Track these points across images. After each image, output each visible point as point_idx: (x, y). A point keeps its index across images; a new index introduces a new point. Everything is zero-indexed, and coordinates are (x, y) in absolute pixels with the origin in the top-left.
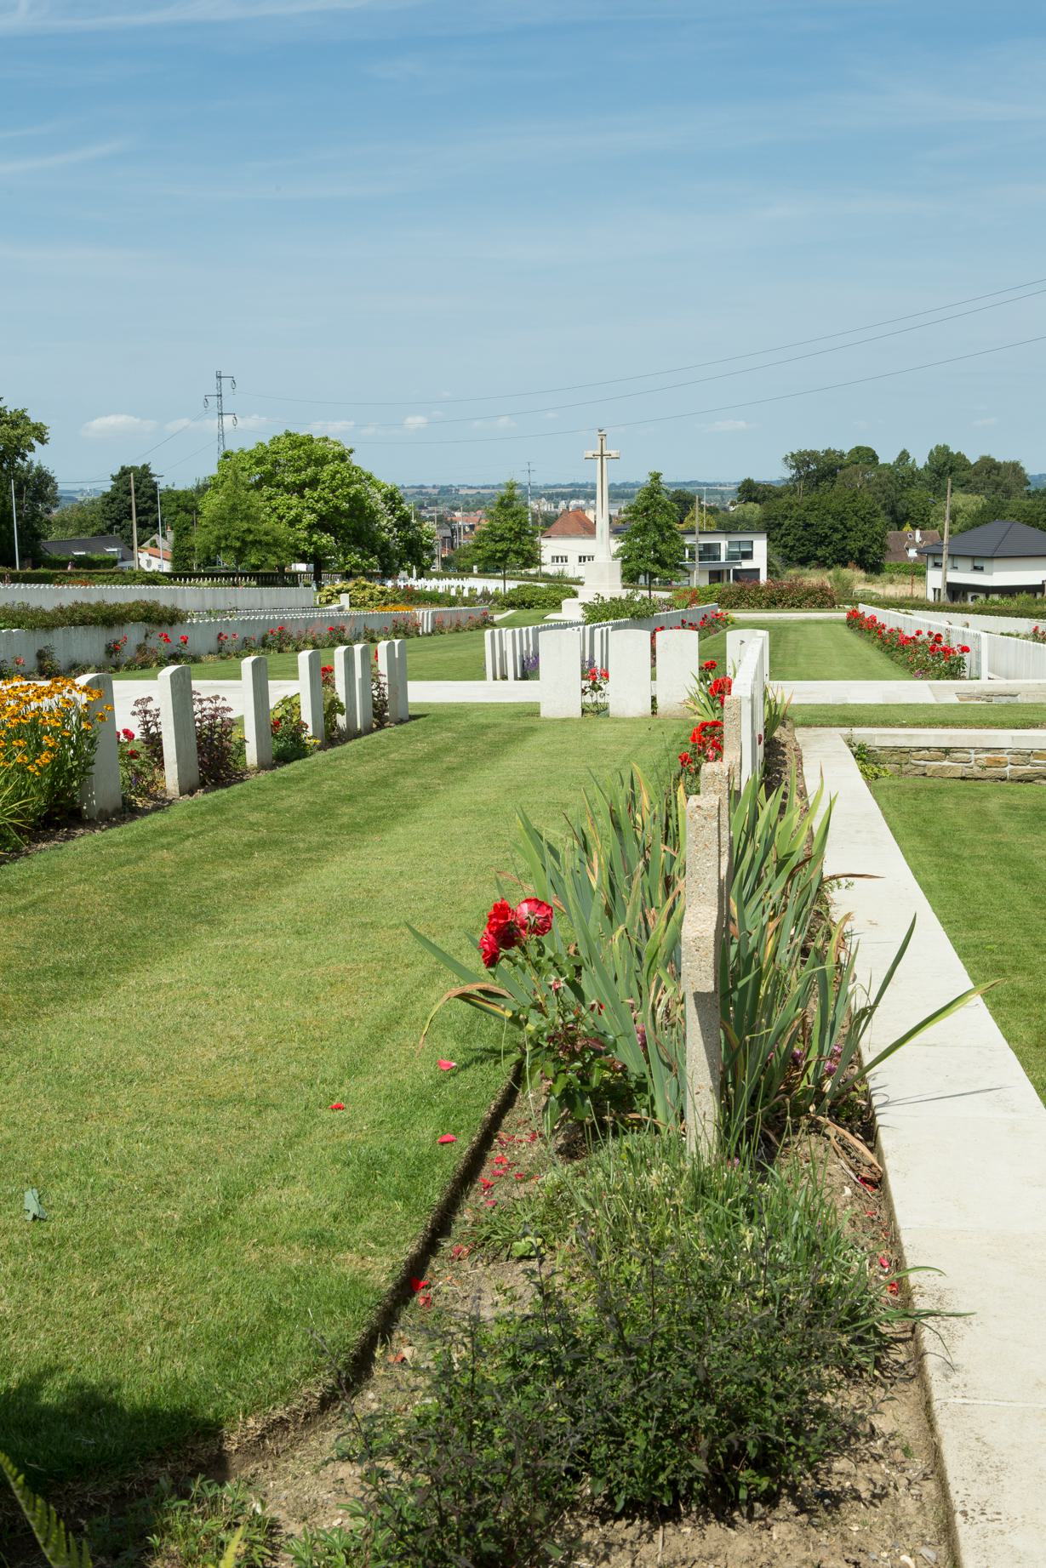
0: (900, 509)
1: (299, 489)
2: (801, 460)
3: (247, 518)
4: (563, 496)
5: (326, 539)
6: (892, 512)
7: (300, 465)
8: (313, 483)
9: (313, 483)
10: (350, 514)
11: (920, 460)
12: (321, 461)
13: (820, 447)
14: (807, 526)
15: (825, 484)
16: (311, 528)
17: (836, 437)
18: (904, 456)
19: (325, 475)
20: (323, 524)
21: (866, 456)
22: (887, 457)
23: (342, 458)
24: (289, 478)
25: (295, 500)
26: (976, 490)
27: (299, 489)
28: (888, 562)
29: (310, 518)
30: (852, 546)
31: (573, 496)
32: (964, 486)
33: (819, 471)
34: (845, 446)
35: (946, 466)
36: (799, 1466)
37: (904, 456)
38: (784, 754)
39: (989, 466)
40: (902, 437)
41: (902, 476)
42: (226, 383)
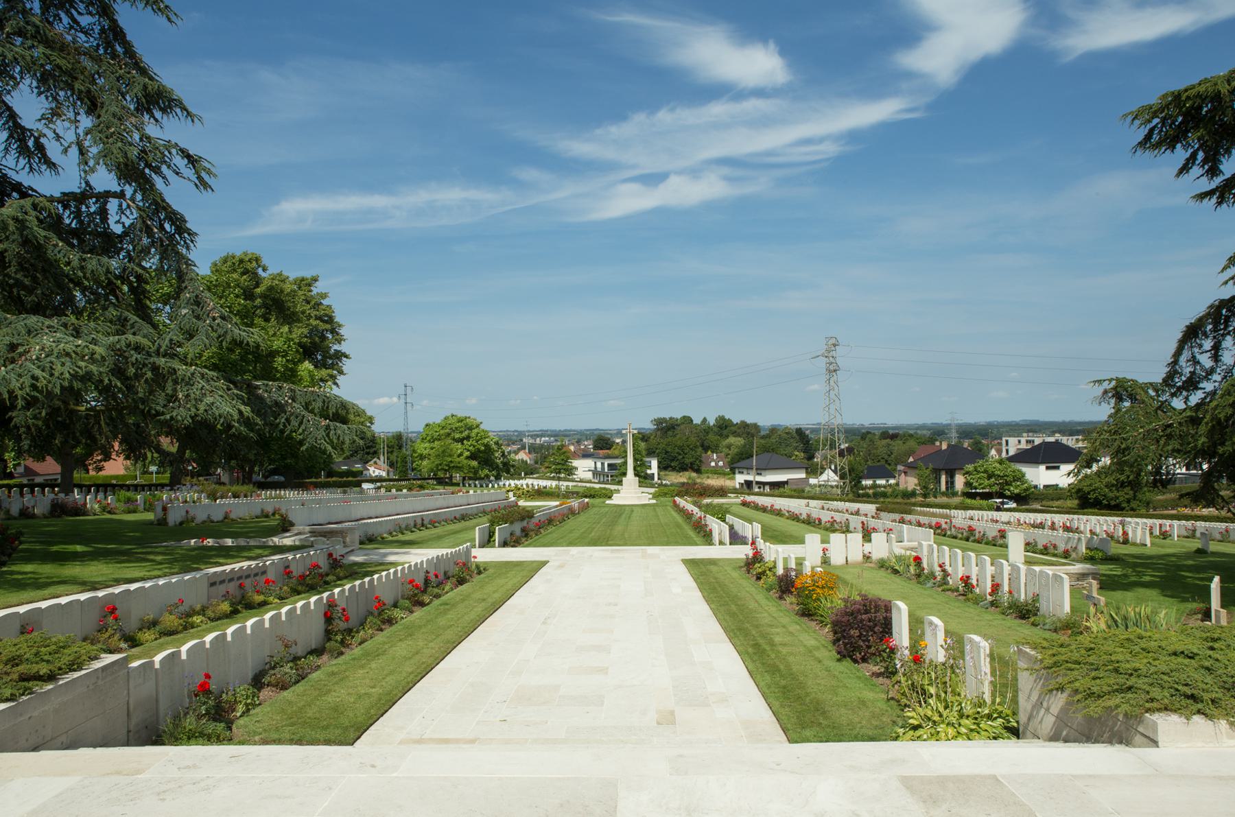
0: (706, 444)
1: (461, 441)
2: (659, 422)
3: (450, 456)
4: (537, 436)
5: (474, 463)
6: (702, 446)
7: (460, 430)
8: (468, 438)
9: (468, 438)
10: (484, 452)
11: (712, 422)
12: (471, 429)
13: (667, 416)
14: (667, 452)
15: (670, 433)
16: (467, 458)
17: (675, 412)
18: (705, 420)
19: (473, 434)
20: (473, 457)
21: (687, 420)
22: (697, 420)
23: (478, 426)
24: (457, 436)
25: (459, 445)
26: (739, 436)
27: (461, 441)
28: (703, 468)
29: (467, 454)
30: (687, 461)
31: (542, 436)
32: (735, 434)
33: (667, 427)
34: (678, 415)
35: (724, 426)
36: (1061, 603)
37: (705, 420)
38: (416, 564)
39: (744, 425)
40: (704, 412)
41: (705, 429)
42: (409, 389)
